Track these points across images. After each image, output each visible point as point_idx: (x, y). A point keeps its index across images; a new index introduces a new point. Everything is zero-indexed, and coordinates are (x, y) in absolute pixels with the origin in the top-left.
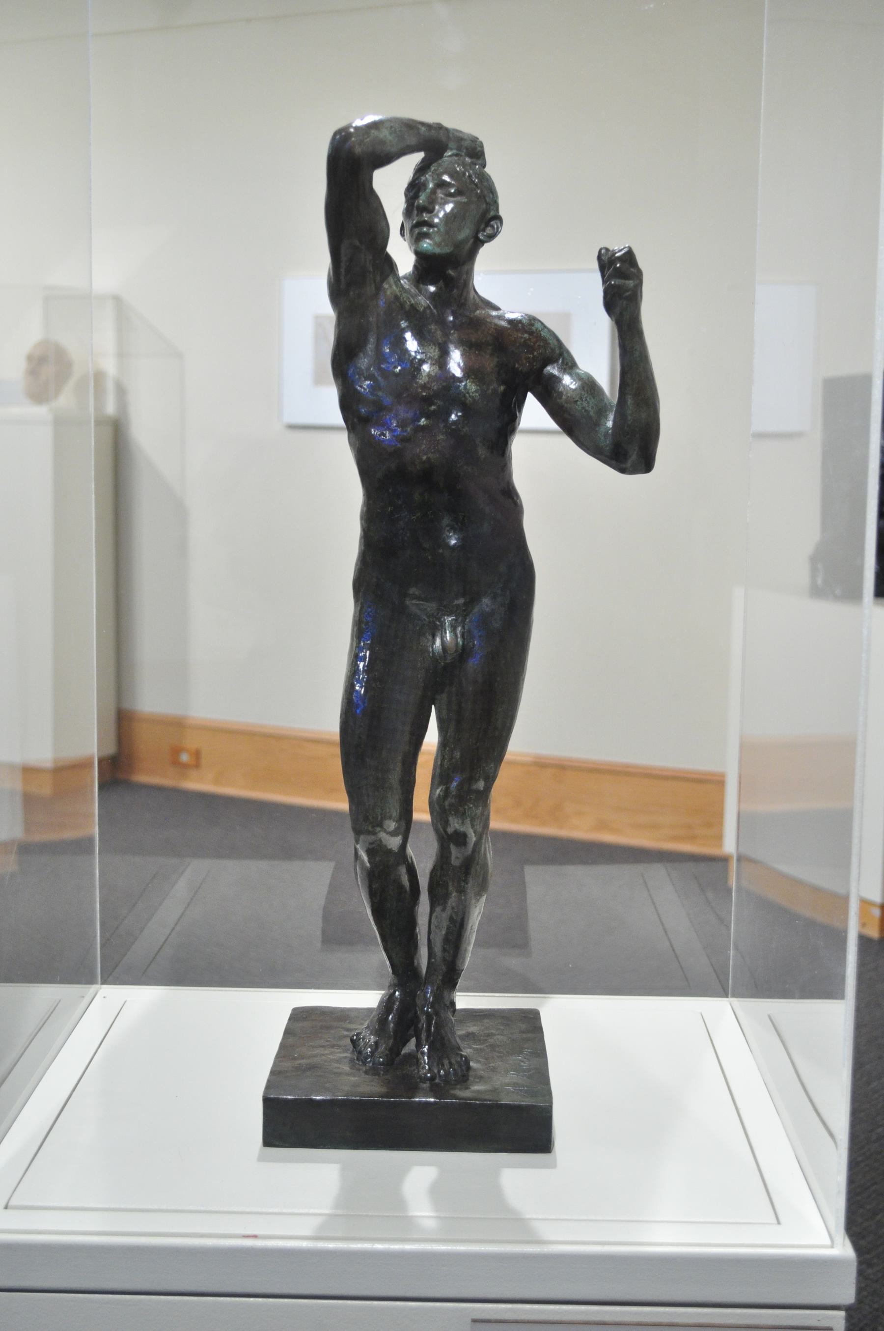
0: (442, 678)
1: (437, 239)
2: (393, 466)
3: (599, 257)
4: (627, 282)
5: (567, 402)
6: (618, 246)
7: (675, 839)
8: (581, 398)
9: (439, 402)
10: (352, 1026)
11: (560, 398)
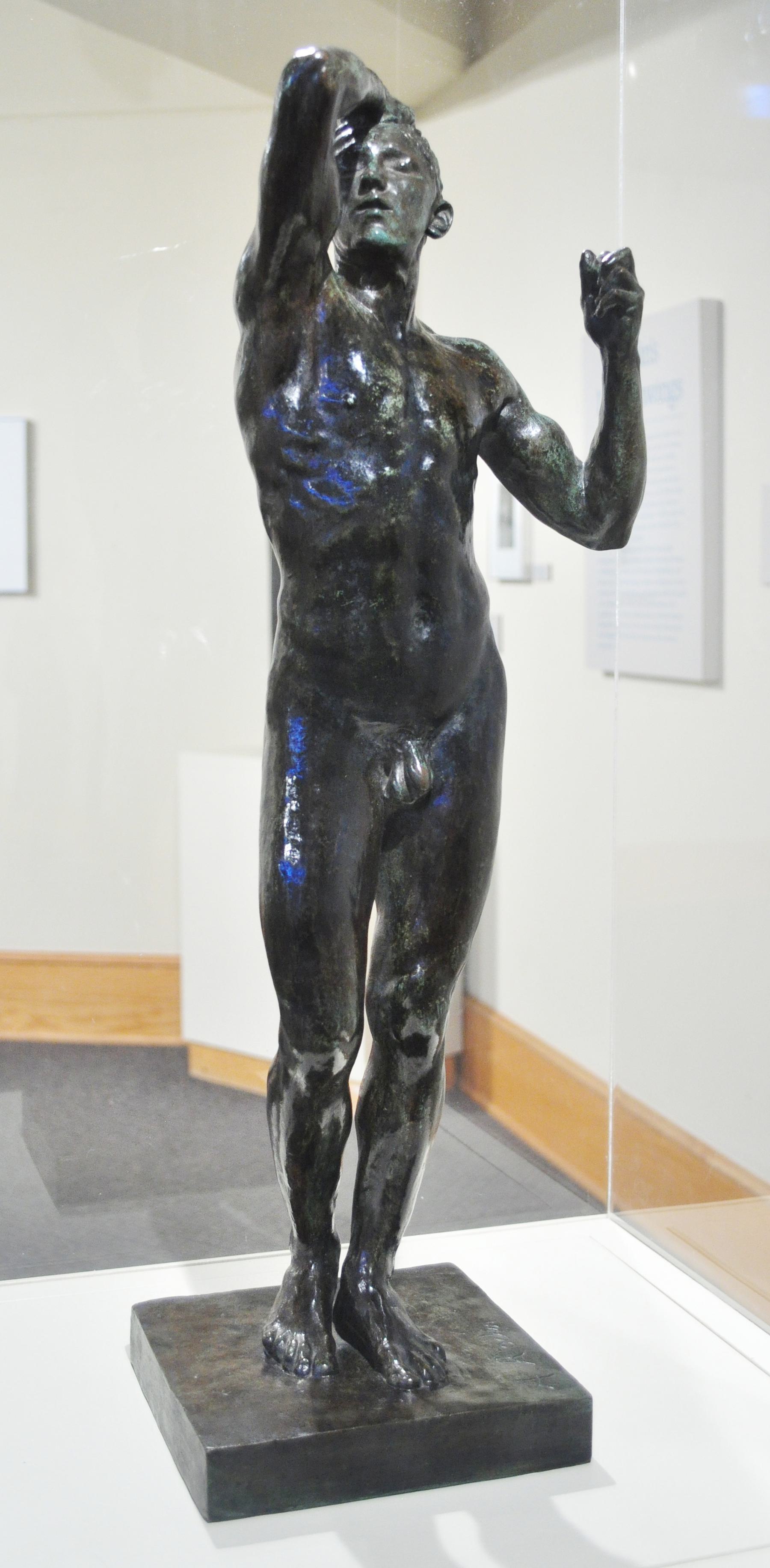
0: (396, 823)
1: (394, 225)
2: (346, 533)
3: (583, 264)
4: (630, 293)
5: (533, 453)
6: (605, 250)
7: (123, 1029)
8: (552, 449)
9: (407, 445)
10: (236, 1322)
11: (525, 449)
